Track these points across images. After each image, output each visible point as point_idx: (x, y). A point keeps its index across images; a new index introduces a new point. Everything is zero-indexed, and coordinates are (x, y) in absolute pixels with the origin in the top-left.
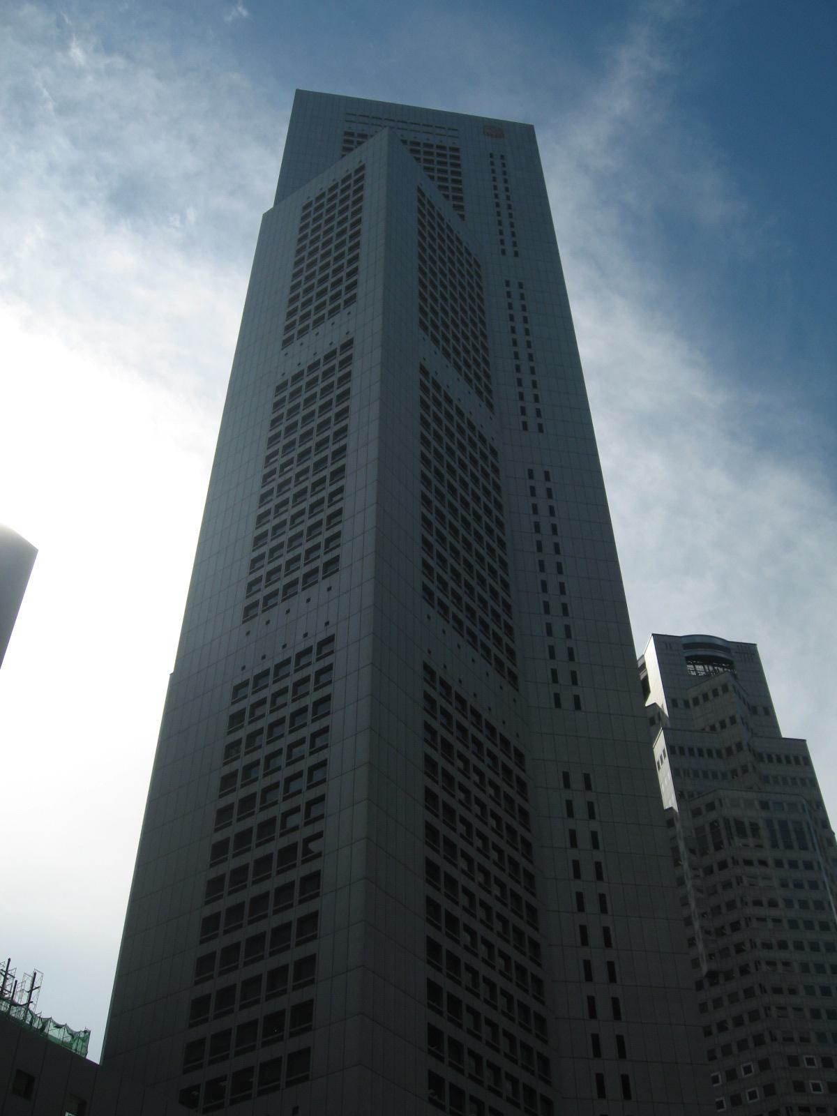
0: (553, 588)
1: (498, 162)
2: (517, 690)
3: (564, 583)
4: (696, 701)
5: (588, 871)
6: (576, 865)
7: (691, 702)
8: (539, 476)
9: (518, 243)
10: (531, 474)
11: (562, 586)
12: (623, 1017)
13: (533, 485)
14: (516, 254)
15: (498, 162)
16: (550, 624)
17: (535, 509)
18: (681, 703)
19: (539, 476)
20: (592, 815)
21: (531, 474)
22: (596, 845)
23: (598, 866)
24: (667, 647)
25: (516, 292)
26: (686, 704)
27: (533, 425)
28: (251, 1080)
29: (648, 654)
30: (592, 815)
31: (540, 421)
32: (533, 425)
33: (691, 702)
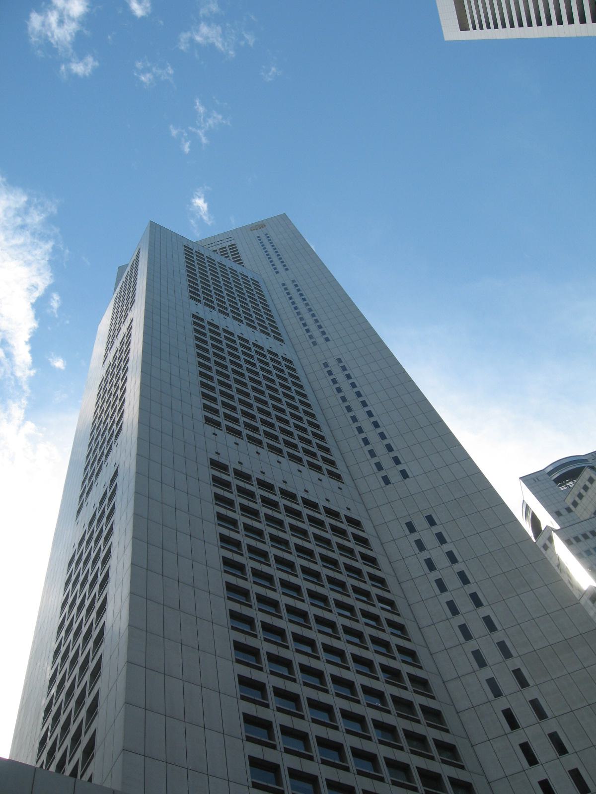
0: (477, 628)
1: (336, 370)
2: (343, 483)
3: (519, 670)
4: (575, 504)
5: (543, 750)
6: (526, 748)
7: (572, 507)
8: (420, 523)
9: (379, 422)
10: (411, 528)
11: (488, 621)
12: (513, 652)
13: (491, 676)
14: (404, 474)
15: (336, 370)
16: (464, 625)
17: (420, 545)
18: (564, 512)
19: (420, 523)
20: (541, 714)
21: (411, 528)
22: (562, 750)
23: (535, 704)
24: (538, 479)
25: (427, 535)
26: (569, 510)
27: (394, 476)
28: (33, 372)
29: (517, 498)
30: (541, 714)
31: (436, 529)
32: (394, 476)
33: (572, 507)
